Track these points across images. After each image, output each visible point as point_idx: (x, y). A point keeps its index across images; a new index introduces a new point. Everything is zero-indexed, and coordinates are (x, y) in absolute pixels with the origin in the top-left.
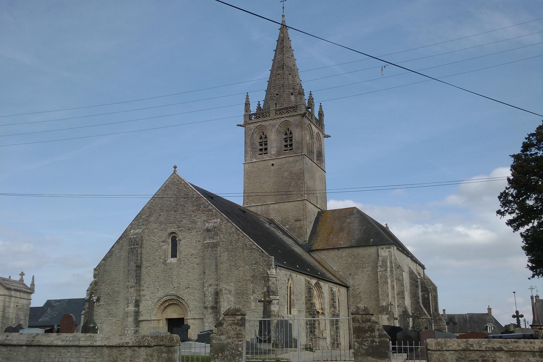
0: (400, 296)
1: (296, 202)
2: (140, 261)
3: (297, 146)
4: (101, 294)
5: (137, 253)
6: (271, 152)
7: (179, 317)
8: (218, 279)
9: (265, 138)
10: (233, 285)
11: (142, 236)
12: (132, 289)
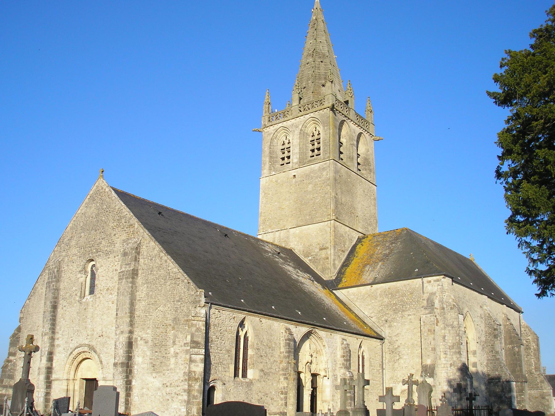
0: (454, 350)
9: (288, 143)
10: (150, 332)
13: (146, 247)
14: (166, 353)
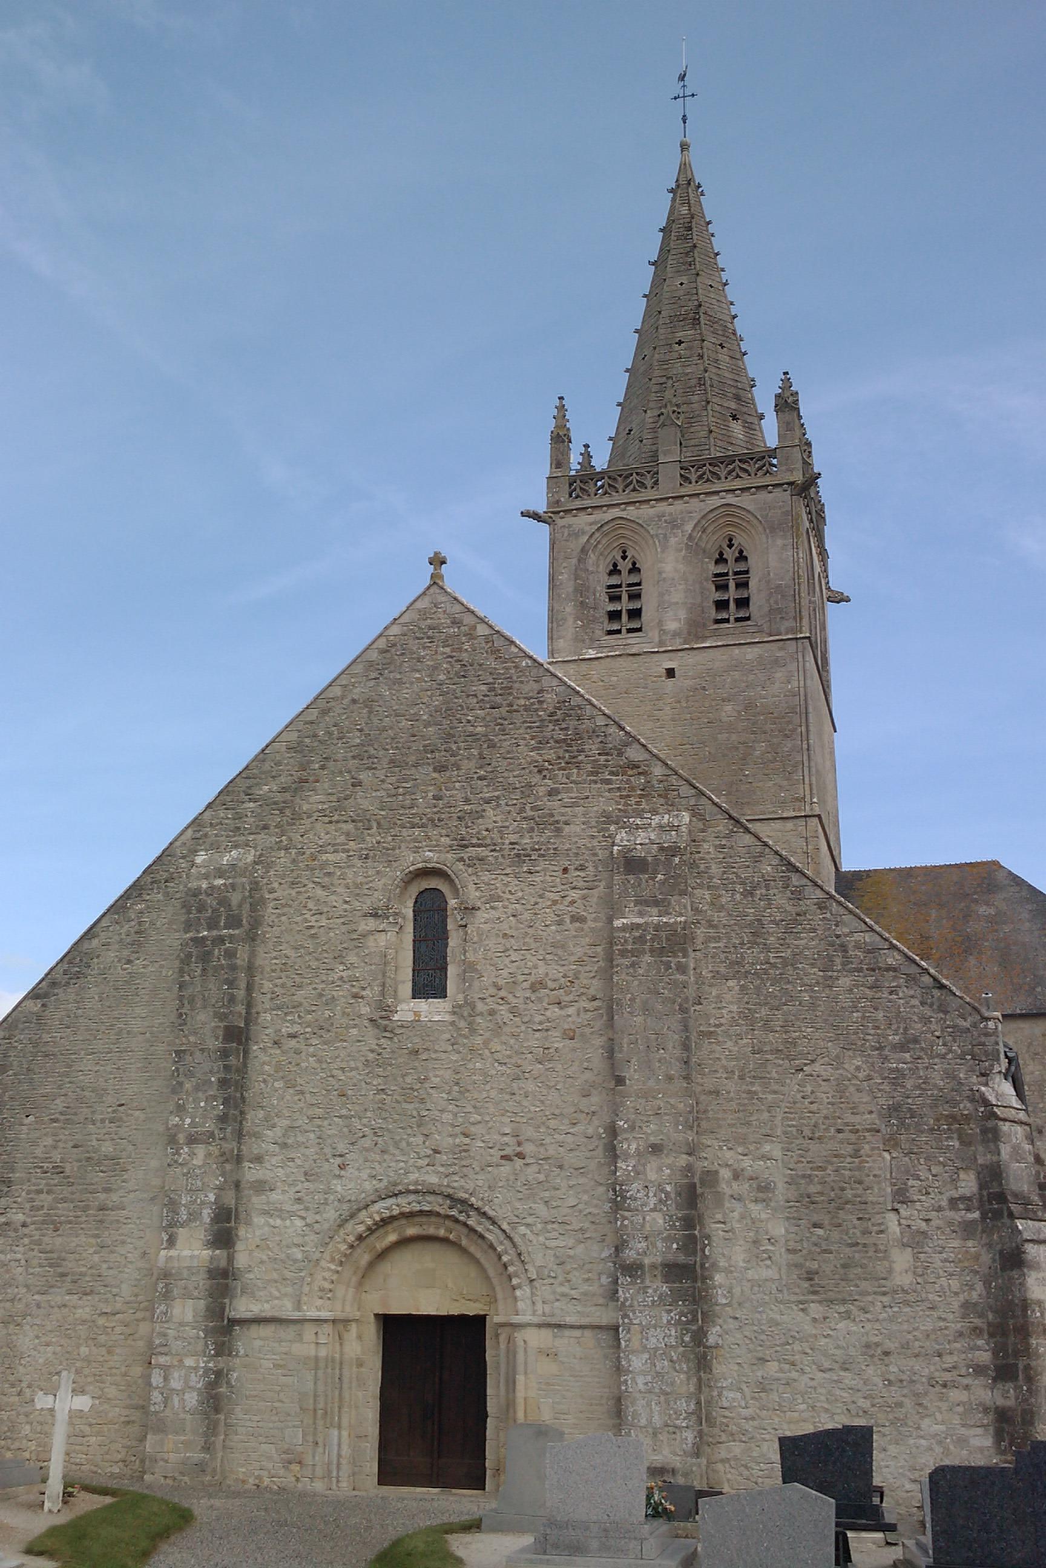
1: (772, 824)
2: (241, 1008)
3: (776, 603)
4: (13, 1171)
5: (233, 968)
6: (660, 623)
7: (455, 1312)
8: (695, 1119)
10: (777, 1153)
11: (257, 883)
12: (201, 1150)
13: (716, 847)
14: (866, 1232)
